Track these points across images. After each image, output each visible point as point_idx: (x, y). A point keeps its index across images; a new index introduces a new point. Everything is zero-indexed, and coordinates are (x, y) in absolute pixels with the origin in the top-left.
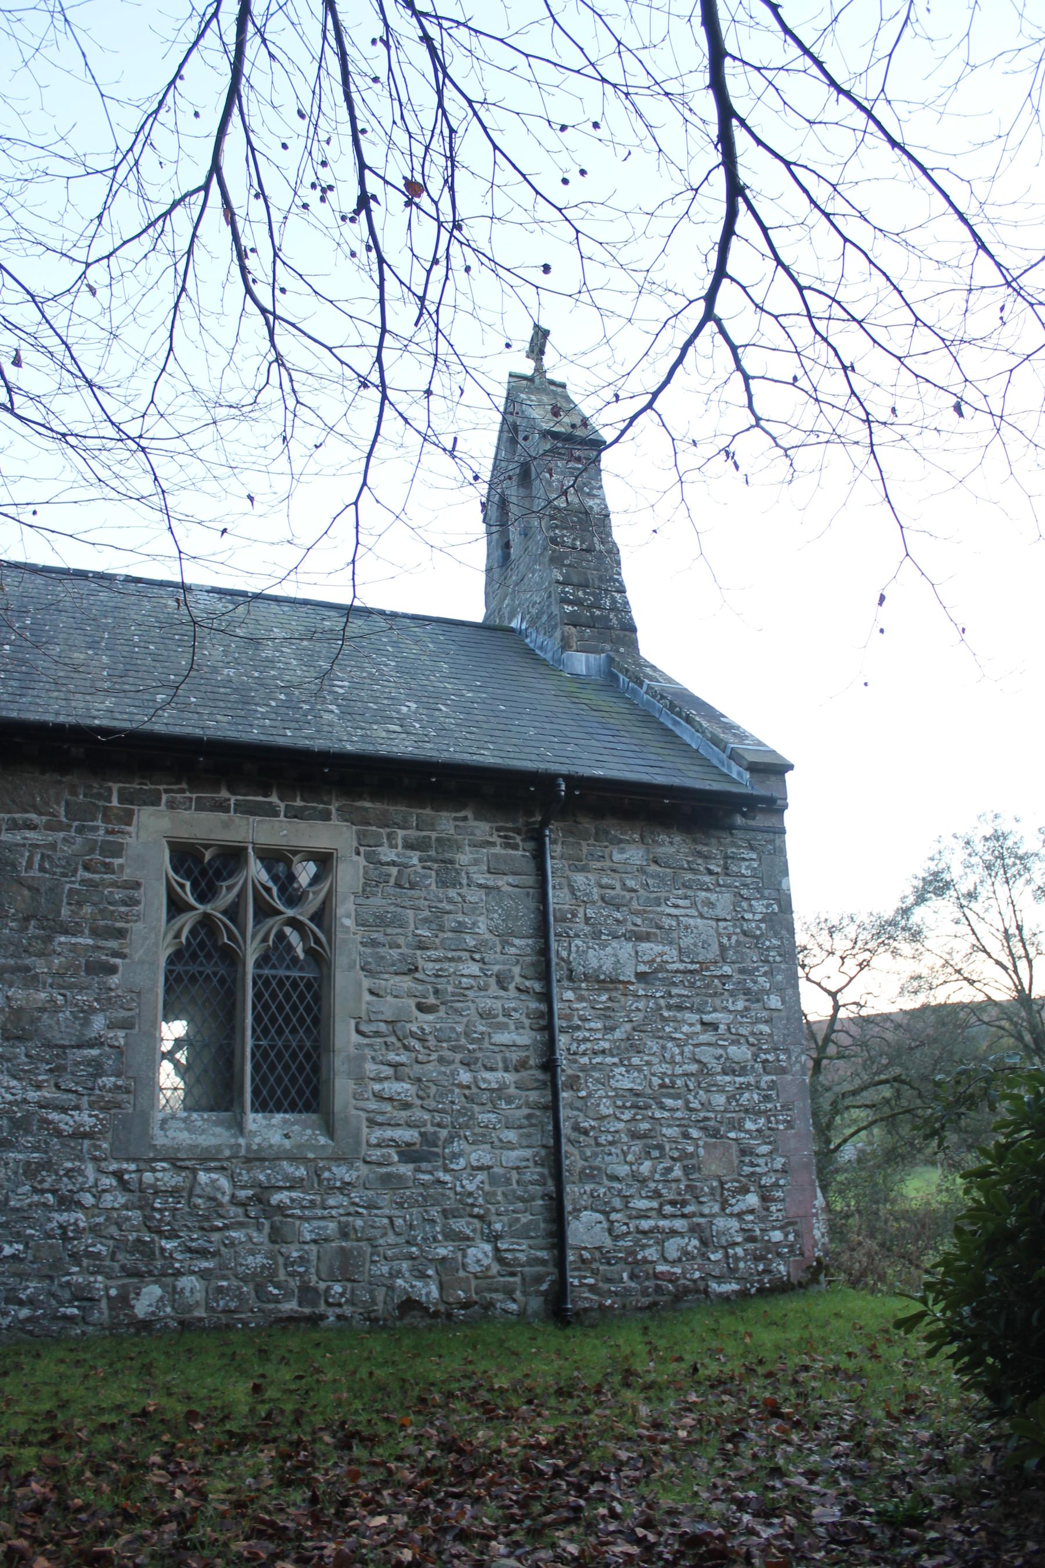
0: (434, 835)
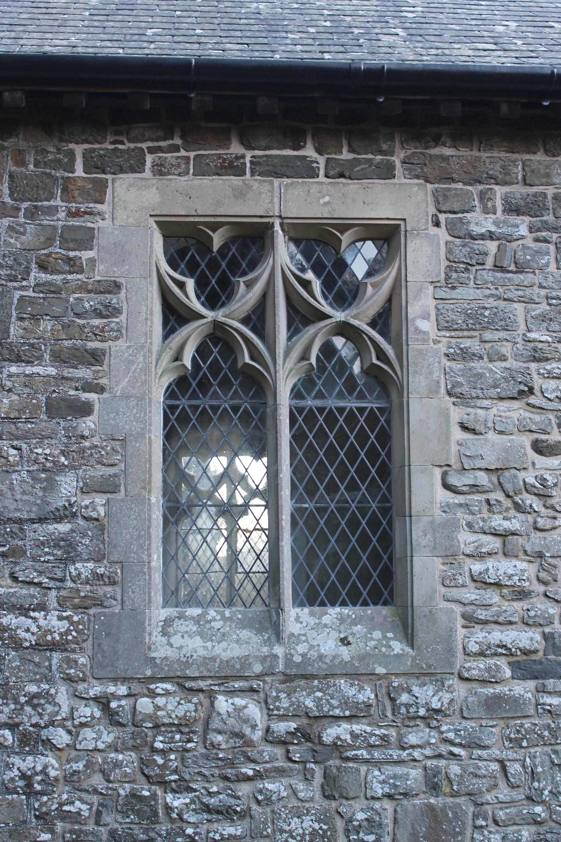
0: (550, 191)
